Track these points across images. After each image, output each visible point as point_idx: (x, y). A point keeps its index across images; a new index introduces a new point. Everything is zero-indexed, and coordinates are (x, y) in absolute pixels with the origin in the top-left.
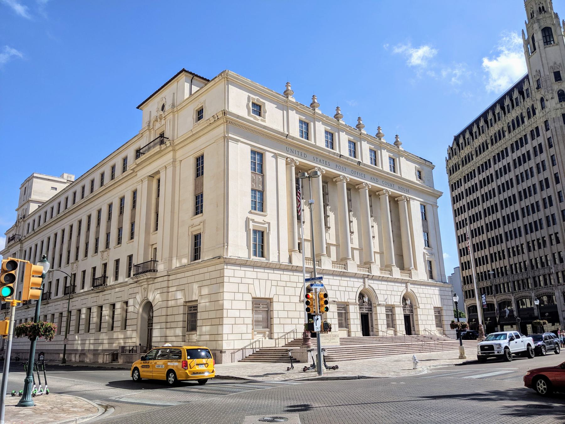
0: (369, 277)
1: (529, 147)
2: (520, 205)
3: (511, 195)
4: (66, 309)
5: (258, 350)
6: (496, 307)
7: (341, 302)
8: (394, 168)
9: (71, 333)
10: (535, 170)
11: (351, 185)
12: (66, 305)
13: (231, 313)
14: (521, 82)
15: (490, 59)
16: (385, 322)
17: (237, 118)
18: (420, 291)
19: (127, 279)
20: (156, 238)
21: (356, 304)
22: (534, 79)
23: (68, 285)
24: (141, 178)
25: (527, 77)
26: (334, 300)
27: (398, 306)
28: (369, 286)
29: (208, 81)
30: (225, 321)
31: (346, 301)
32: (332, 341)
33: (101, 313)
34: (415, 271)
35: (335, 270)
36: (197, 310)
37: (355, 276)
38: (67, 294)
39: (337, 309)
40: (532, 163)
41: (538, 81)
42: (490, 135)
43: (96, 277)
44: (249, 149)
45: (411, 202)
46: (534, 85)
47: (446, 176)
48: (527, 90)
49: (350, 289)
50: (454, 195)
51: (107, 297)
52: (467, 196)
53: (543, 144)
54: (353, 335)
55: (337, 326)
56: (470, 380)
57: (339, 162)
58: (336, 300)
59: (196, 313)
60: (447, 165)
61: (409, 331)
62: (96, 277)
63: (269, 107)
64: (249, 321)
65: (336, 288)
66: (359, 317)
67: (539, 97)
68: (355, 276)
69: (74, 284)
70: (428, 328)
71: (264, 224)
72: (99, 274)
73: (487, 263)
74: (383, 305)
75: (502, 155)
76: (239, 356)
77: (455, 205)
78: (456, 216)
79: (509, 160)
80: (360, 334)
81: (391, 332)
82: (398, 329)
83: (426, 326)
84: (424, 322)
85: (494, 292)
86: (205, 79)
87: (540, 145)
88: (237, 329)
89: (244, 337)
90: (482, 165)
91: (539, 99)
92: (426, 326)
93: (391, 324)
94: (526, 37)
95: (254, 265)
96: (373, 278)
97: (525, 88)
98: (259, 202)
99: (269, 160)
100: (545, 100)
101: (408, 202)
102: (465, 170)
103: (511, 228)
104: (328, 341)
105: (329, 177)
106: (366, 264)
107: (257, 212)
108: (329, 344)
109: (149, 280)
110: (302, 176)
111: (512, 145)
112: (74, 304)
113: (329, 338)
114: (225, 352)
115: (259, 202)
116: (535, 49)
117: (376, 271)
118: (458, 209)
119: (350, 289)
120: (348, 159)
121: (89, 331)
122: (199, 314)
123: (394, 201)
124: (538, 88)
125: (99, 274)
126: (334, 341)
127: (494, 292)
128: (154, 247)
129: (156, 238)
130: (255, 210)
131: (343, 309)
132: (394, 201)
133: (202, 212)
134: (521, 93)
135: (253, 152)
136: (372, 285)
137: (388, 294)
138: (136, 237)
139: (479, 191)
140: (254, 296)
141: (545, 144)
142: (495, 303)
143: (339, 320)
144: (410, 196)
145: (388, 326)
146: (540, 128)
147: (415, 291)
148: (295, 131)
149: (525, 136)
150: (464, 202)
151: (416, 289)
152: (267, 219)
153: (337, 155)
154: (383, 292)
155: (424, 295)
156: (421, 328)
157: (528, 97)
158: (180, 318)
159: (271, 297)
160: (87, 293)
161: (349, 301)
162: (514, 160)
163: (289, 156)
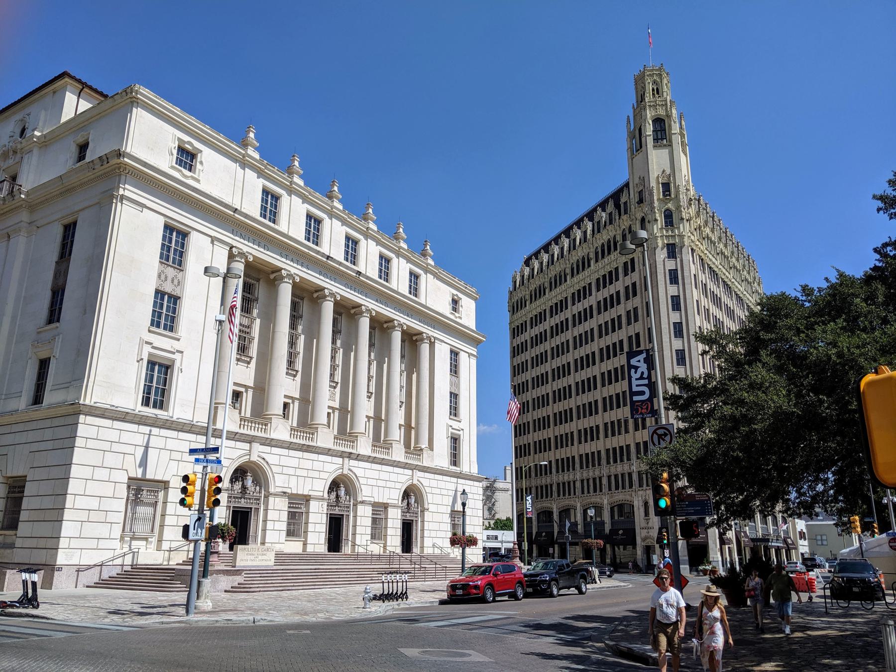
0: (352, 456)
1: (618, 286)
2: (600, 369)
3: (590, 352)
5: (129, 568)
6: (556, 517)
7: (297, 495)
8: (414, 289)
11: (344, 307)
13: (81, 502)
14: (620, 191)
16: (369, 530)
17: (144, 166)
18: (434, 483)
21: (323, 499)
22: (636, 190)
25: (627, 185)
26: (285, 490)
27: (395, 506)
28: (350, 470)
29: (106, 96)
30: (67, 514)
31: (306, 493)
32: (260, 557)
34: (429, 452)
35: (295, 441)
36: (23, 492)
37: (328, 452)
40: (620, 310)
41: (640, 193)
42: (572, 261)
44: (161, 221)
45: (437, 345)
46: (634, 197)
47: (507, 316)
48: (625, 203)
49: (316, 474)
50: (515, 345)
52: (575, 348)
53: (638, 284)
54: (310, 549)
55: (284, 533)
56: (429, 629)
57: (325, 266)
58: (289, 491)
59: (21, 498)
60: (510, 299)
61: (407, 544)
63: (208, 156)
65: (291, 471)
66: (324, 519)
67: (639, 216)
68: (328, 452)
70: (439, 542)
71: (174, 353)
73: (550, 450)
74: (369, 503)
75: (583, 293)
76: (92, 577)
77: (515, 359)
78: (514, 375)
79: (592, 301)
80: (322, 548)
81: (294, 547)
82: (389, 543)
83: (435, 540)
84: (433, 534)
85: (555, 494)
86: (101, 94)
87: (634, 284)
88: (90, 530)
89: (103, 544)
90: (556, 304)
91: (639, 218)
92: (435, 540)
93: (378, 530)
94: (632, 128)
95: (141, 421)
96: (358, 457)
97: (623, 200)
99: (463, 357)
100: (646, 220)
101: (432, 345)
102: (533, 309)
103: (585, 401)
104: (252, 557)
105: (307, 290)
106: (345, 433)
107: (161, 331)
108: (255, 563)
110: (257, 281)
111: (598, 280)
113: (256, 553)
114: (60, 569)
116: (641, 147)
117: (364, 447)
118: (558, 368)
119: (316, 474)
120: (340, 264)
122: (25, 500)
123: (412, 340)
124: (641, 201)
126: (264, 557)
127: (555, 494)
130: (158, 326)
131: (297, 508)
132: (412, 340)
133: (58, 321)
134: (617, 206)
135: (451, 351)
136: (421, 479)
137: (379, 484)
139: (548, 342)
141: (641, 284)
142: (555, 510)
143: (289, 524)
144: (435, 335)
145: (373, 537)
146: (636, 260)
147: (425, 482)
148: (252, 206)
149: (617, 269)
150: (527, 356)
151: (425, 481)
153: (323, 255)
154: (371, 482)
155: (438, 491)
156: (428, 542)
157: (626, 213)
159: (165, 479)
161: (311, 493)
162: (599, 303)
163: (234, 244)
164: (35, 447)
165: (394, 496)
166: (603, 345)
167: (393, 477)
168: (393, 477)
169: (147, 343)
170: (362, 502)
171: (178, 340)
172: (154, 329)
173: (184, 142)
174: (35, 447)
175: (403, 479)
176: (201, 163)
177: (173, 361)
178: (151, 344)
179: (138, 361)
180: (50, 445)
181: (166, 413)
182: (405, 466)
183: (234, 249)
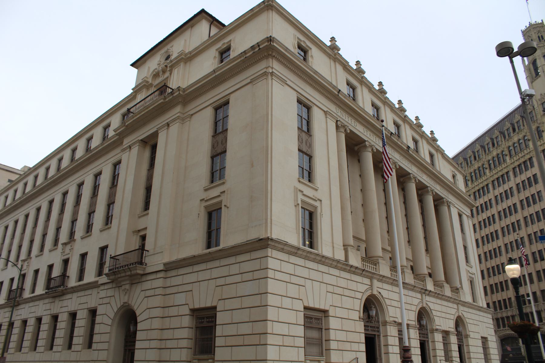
4: (8, 320)
9: (10, 351)
10: (493, 202)
12: (8, 315)
15: (513, 50)
17: (286, 51)
19: (97, 279)
20: (149, 222)
21: (416, 327)
23: (15, 287)
24: (129, 144)
28: (427, 304)
30: (271, 340)
33: (39, 328)
38: (11, 299)
39: (397, 333)
43: (53, 276)
51: (65, 303)
62: (53, 276)
64: (301, 342)
69: (22, 287)
71: (316, 201)
72: (56, 272)
98: (308, 174)
99: (317, 116)
109: (516, 151)
112: (19, 312)
115: (308, 174)
117: (384, 270)
121: (35, 350)
125: (56, 272)
128: (142, 233)
129: (149, 222)
138: (115, 222)
140: (306, 305)
152: (318, 195)
158: (185, 333)
160: (40, 298)
164: (221, 282)
165: (410, 317)
166: (500, 208)
167: (353, 285)
168: (353, 285)
169: (300, 191)
170: (437, 330)
171: (317, 190)
172: (301, 180)
173: (301, 40)
174: (221, 282)
175: (362, 288)
176: (312, 56)
177: (316, 208)
178: (302, 192)
179: (296, 206)
180: (238, 278)
181: (317, 252)
182: (362, 272)
183: (339, 123)
